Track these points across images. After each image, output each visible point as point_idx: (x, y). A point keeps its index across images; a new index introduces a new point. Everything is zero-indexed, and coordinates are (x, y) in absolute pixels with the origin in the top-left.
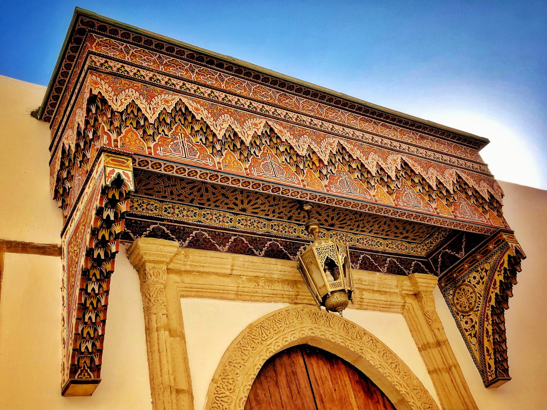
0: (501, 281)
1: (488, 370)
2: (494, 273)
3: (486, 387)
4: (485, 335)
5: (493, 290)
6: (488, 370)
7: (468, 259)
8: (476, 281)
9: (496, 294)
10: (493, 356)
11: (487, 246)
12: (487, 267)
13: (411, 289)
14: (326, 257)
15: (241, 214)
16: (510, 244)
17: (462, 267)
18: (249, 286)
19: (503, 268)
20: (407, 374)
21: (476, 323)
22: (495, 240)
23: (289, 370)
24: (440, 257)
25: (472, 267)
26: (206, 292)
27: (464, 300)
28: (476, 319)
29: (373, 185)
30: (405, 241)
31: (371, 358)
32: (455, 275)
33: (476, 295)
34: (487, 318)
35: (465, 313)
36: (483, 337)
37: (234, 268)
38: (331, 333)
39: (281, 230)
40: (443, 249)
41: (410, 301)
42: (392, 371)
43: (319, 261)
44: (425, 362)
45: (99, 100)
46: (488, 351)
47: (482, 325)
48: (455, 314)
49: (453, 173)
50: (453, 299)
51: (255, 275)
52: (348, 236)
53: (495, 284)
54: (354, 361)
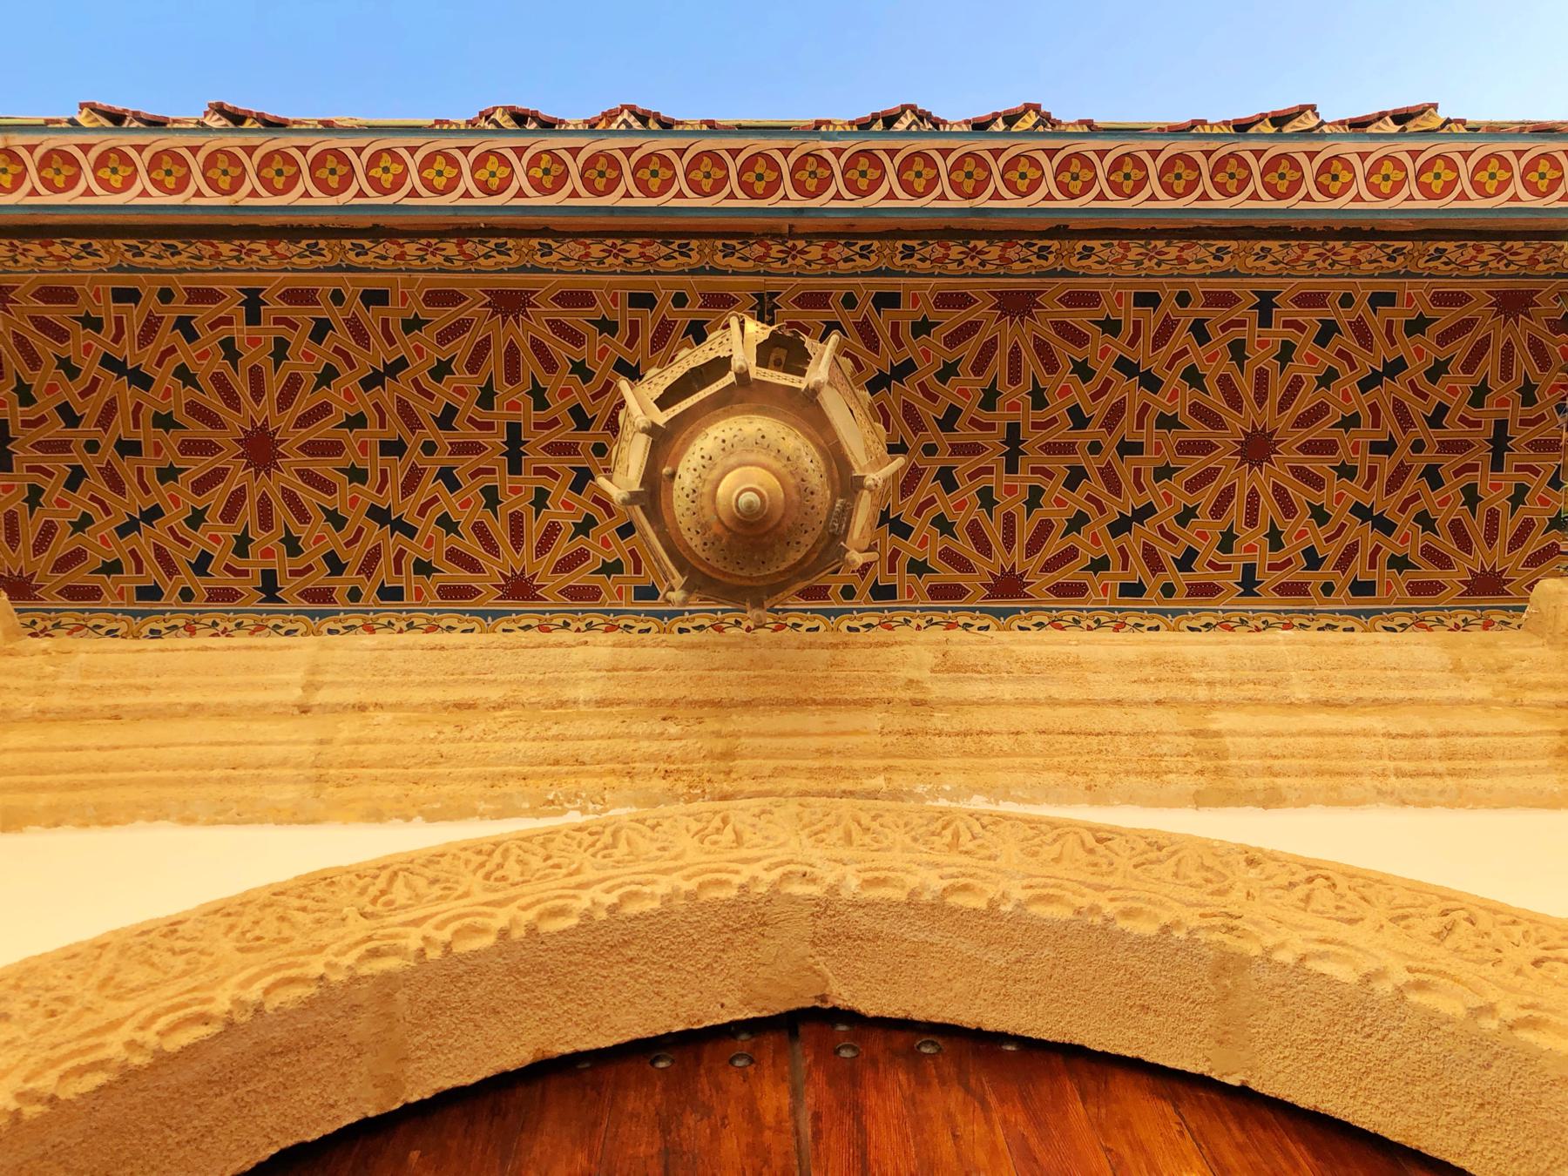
26: (122, 783)
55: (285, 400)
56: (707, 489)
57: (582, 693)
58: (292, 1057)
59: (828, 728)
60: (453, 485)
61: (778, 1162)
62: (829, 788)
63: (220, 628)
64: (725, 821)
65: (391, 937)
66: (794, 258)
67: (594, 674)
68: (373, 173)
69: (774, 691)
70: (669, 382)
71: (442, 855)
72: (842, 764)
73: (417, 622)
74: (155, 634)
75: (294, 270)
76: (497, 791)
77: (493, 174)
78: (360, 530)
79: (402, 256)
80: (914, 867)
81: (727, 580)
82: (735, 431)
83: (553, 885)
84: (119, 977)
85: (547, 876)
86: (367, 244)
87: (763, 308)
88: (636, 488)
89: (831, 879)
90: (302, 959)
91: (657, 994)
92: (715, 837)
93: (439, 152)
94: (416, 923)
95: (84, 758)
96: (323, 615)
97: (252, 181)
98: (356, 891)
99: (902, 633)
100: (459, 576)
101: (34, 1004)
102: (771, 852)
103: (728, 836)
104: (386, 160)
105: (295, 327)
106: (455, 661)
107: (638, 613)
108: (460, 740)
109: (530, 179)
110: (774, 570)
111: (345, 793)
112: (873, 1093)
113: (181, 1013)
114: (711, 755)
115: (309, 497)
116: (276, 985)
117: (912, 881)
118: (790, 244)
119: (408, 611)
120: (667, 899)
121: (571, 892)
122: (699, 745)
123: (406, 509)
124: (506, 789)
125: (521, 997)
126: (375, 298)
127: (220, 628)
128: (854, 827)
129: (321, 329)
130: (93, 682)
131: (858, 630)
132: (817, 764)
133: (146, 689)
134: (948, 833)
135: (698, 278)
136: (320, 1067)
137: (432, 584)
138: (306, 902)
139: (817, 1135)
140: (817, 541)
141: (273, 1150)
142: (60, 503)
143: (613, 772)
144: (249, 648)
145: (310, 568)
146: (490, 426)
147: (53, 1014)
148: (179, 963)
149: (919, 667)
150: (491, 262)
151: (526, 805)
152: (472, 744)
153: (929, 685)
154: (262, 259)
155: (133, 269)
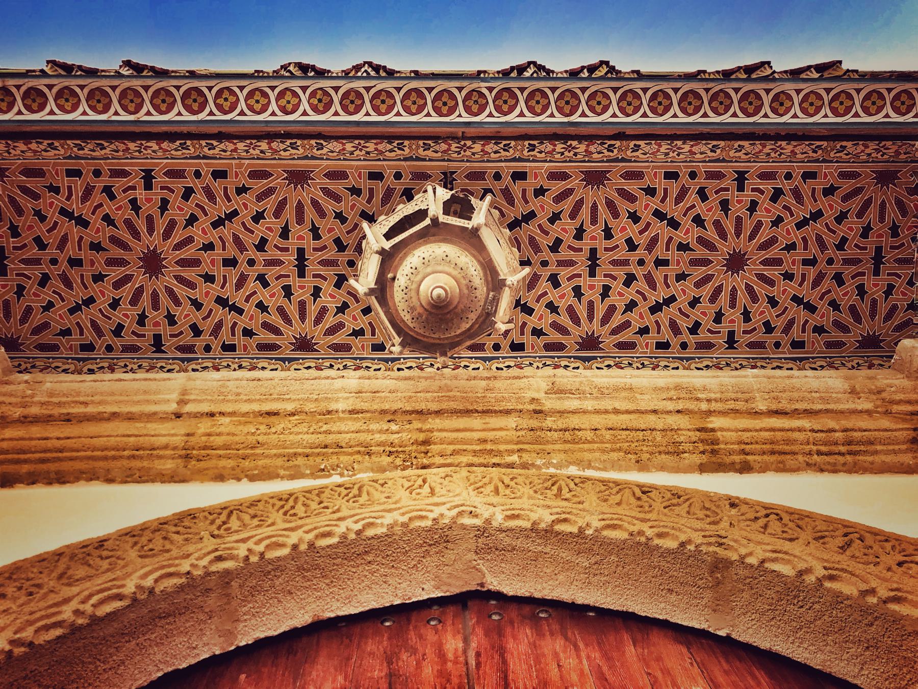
55: (167, 234)
56: (414, 286)
57: (341, 406)
58: (171, 619)
59: (485, 426)
60: (265, 284)
61: (455, 681)
62: (485, 462)
63: (129, 368)
64: (424, 481)
65: (229, 549)
66: (465, 151)
67: (348, 395)
68: (218, 101)
69: (453, 405)
70: (392, 224)
71: (259, 501)
72: (493, 447)
73: (244, 364)
74: (91, 371)
75: (172, 158)
76: (291, 463)
77: (289, 102)
78: (211, 311)
79: (235, 150)
80: (535, 508)
81: (425, 339)
82: (430, 253)
83: (324, 518)
84: (70, 572)
85: (320, 513)
86: (215, 143)
87: (447, 180)
88: (373, 286)
89: (486, 515)
90: (177, 562)
91: (385, 582)
92: (418, 491)
93: (257, 89)
94: (244, 541)
95: (49, 444)
96: (189, 360)
97: (147, 106)
98: (208, 522)
99: (528, 371)
100: (270, 338)
101: (20, 588)
102: (452, 499)
103: (426, 489)
104: (226, 94)
105: (173, 192)
106: (266, 388)
107: (373, 359)
108: (269, 434)
109: (311, 105)
110: (453, 334)
111: (202, 465)
112: (511, 640)
113: (106, 594)
114: (416, 443)
115: (181, 291)
116: (162, 577)
117: (534, 516)
118: (462, 143)
119: (239, 358)
120: (391, 527)
121: (334, 523)
122: (409, 437)
123: (238, 298)
124: (296, 463)
125: (305, 584)
126: (220, 174)
127: (129, 368)
128: (500, 485)
129: (188, 193)
130: (55, 400)
131: (502, 369)
132: (478, 448)
133: (85, 404)
134: (555, 488)
135: (408, 163)
136: (187, 625)
137: (253, 342)
138: (179, 529)
139: (478, 665)
140: (479, 317)
141: (160, 674)
142: (35, 295)
143: (359, 452)
144: (146, 380)
145: (181, 333)
146: (287, 250)
147: (31, 594)
148: (105, 564)
149: (538, 391)
150: (287, 153)
151: (308, 472)
152: (276, 436)
153: (544, 402)
154: (154, 151)
155: (78, 157)
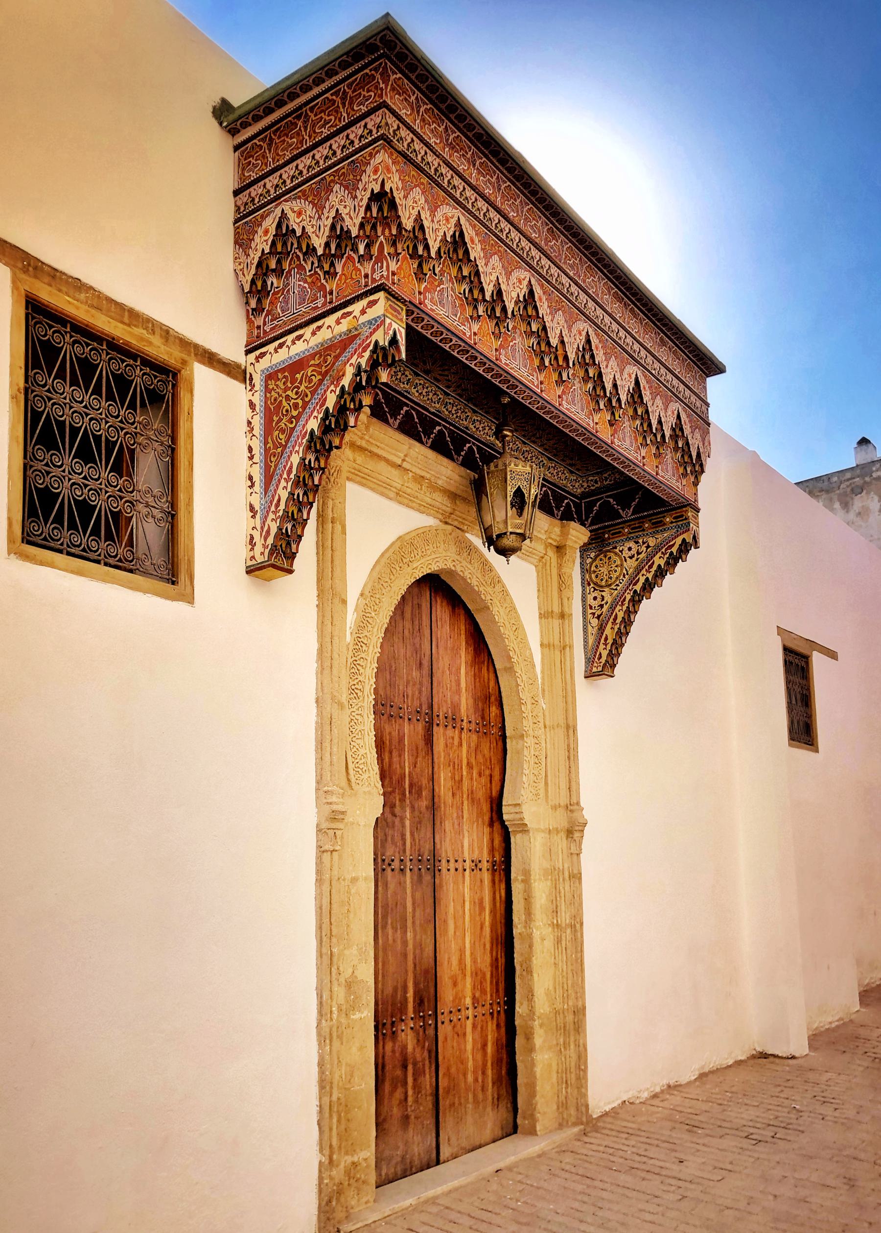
0: (659, 566)
1: (596, 660)
2: (657, 553)
3: (586, 677)
4: (611, 620)
5: (645, 573)
6: (596, 660)
7: (633, 523)
8: (630, 554)
9: (647, 578)
10: (609, 647)
11: (664, 517)
12: (652, 542)
13: (558, 539)
14: (517, 486)
15: (422, 376)
16: (691, 525)
17: (621, 530)
18: (413, 487)
19: (669, 551)
20: (523, 641)
21: (607, 603)
22: (676, 513)
23: (415, 602)
24: (597, 505)
25: (632, 535)
27: (604, 570)
28: (608, 598)
29: (399, 251)
30: (412, 370)
31: (497, 613)
32: (607, 536)
33: (622, 570)
34: (622, 603)
35: (598, 587)
36: (608, 622)
37: (407, 459)
38: (470, 571)
39: (453, 412)
40: (607, 497)
41: (551, 553)
42: (511, 634)
43: (509, 488)
44: (541, 632)
45: (387, 201)
46: (606, 639)
47: (612, 608)
48: (585, 583)
49: (452, 218)
50: (591, 564)
51: (422, 475)
52: (517, 443)
53: (651, 567)
54: (477, 610)
